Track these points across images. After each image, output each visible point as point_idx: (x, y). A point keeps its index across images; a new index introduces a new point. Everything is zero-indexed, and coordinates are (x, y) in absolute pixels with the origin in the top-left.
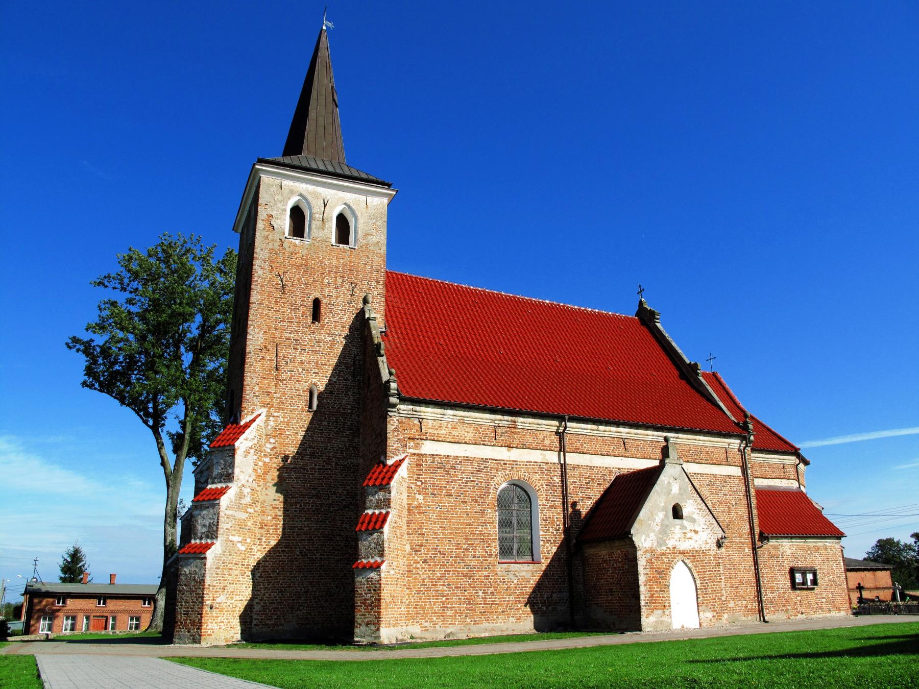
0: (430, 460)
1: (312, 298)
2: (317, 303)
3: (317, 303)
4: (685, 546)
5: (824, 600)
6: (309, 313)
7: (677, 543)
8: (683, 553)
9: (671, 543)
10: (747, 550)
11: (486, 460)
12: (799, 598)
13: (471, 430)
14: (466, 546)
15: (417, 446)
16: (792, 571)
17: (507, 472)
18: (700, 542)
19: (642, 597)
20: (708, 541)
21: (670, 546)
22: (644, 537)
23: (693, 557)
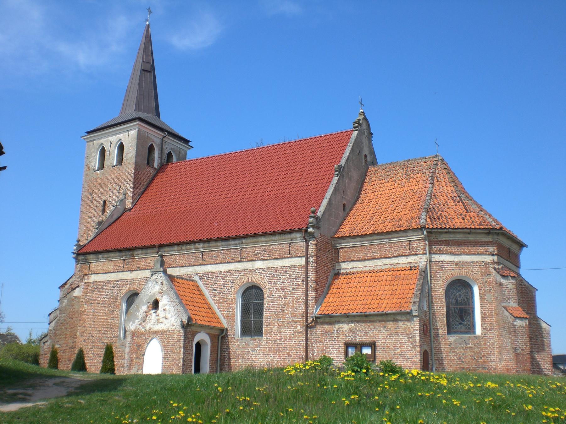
0: (92, 284)
1: (103, 200)
2: (105, 201)
3: (105, 201)
4: (158, 328)
6: (101, 209)
7: (152, 326)
8: (156, 333)
10: (299, 328)
11: (118, 281)
14: (103, 332)
15: (88, 279)
16: (348, 345)
17: (128, 286)
18: (169, 325)
20: (175, 324)
21: (147, 328)
22: (131, 323)
23: (163, 335)
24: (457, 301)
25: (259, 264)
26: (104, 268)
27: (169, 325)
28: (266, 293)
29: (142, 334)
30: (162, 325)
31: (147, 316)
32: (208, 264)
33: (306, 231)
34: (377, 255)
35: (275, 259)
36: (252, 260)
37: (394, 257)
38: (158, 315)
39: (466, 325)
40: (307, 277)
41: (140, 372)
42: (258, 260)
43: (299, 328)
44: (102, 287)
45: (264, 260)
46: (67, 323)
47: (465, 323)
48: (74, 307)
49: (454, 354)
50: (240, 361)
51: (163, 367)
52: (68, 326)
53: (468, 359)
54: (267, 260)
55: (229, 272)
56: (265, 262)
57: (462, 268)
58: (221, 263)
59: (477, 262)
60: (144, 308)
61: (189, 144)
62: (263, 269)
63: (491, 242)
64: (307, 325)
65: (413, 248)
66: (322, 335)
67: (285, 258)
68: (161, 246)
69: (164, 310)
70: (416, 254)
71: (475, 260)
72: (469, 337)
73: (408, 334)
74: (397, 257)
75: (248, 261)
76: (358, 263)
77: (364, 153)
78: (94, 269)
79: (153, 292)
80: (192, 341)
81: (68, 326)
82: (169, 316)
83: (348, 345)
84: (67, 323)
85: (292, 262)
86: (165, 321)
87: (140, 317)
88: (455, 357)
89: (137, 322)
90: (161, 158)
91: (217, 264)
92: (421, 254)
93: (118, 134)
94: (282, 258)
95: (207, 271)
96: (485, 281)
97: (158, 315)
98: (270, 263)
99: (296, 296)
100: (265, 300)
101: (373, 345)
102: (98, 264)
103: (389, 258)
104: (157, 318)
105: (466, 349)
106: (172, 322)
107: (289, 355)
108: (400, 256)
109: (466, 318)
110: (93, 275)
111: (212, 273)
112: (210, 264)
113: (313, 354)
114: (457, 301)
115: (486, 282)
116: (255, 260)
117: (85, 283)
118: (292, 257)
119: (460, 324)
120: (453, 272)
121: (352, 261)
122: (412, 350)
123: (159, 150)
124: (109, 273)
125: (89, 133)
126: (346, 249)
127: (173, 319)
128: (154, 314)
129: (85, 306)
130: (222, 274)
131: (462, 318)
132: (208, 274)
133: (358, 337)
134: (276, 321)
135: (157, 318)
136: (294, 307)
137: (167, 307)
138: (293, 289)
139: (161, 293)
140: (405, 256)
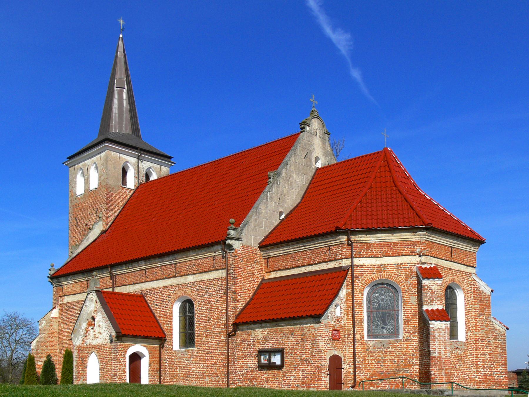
4: (95, 342)
5: (292, 378)
7: (91, 341)
8: (94, 347)
9: (88, 341)
10: (222, 338)
12: (265, 376)
13: (79, 286)
19: (74, 374)
23: (98, 348)
24: (379, 305)
25: (190, 279)
26: (73, 289)
27: (102, 339)
28: (196, 306)
29: (84, 348)
30: (98, 339)
31: (87, 332)
32: (150, 281)
33: (225, 243)
34: (301, 262)
35: (202, 272)
36: (185, 275)
37: (315, 264)
38: (94, 331)
39: (389, 329)
40: (227, 288)
41: (85, 383)
42: (189, 274)
43: (222, 338)
44: (73, 308)
45: (194, 274)
46: (47, 342)
47: (388, 327)
48: (53, 327)
49: (372, 358)
50: (178, 370)
51: (101, 379)
52: (48, 344)
53: (388, 363)
54: (196, 273)
55: (167, 287)
56: (195, 276)
57: (384, 272)
58: (160, 279)
59: (401, 264)
60: (85, 325)
61: (172, 160)
62: (193, 283)
63: (418, 242)
64: (228, 335)
65: (333, 253)
66: (241, 344)
67: (211, 271)
68: (113, 266)
69: (99, 326)
70: (335, 260)
71: (400, 262)
72: (389, 341)
73: (312, 340)
74: (318, 263)
75: (181, 276)
76: (284, 271)
77: (314, 155)
78: (66, 291)
79: (90, 310)
80: (125, 353)
81: (48, 344)
82: (102, 331)
83: (261, 352)
84: (47, 342)
85: (217, 275)
86: (100, 336)
87: (82, 333)
88: (373, 362)
89: (81, 338)
90: (138, 177)
91: (157, 280)
92: (339, 260)
93: (93, 157)
94: (208, 271)
95: (150, 287)
96: (409, 283)
97: (94, 331)
98: (199, 276)
99: (220, 308)
100: (195, 312)
101: (281, 352)
102: (68, 284)
103: (312, 265)
104: (94, 333)
105: (386, 352)
106: (105, 337)
107: (216, 363)
108: (321, 262)
109: (389, 322)
110: (66, 297)
111: (154, 289)
112: (152, 281)
113: (234, 362)
114: (379, 305)
115: (410, 284)
116: (187, 275)
117: (61, 304)
118: (216, 270)
119: (383, 328)
120: (373, 275)
121: (279, 270)
122: (315, 356)
123: (135, 170)
124: (77, 294)
125: (70, 158)
126: (274, 259)
127: (105, 333)
128: (92, 331)
129: (62, 325)
130: (162, 290)
131: (384, 322)
132: (150, 290)
133: (270, 345)
134: (204, 332)
135: (94, 333)
136: (218, 318)
137: (100, 324)
138: (217, 301)
139: (96, 311)
140: (325, 262)
